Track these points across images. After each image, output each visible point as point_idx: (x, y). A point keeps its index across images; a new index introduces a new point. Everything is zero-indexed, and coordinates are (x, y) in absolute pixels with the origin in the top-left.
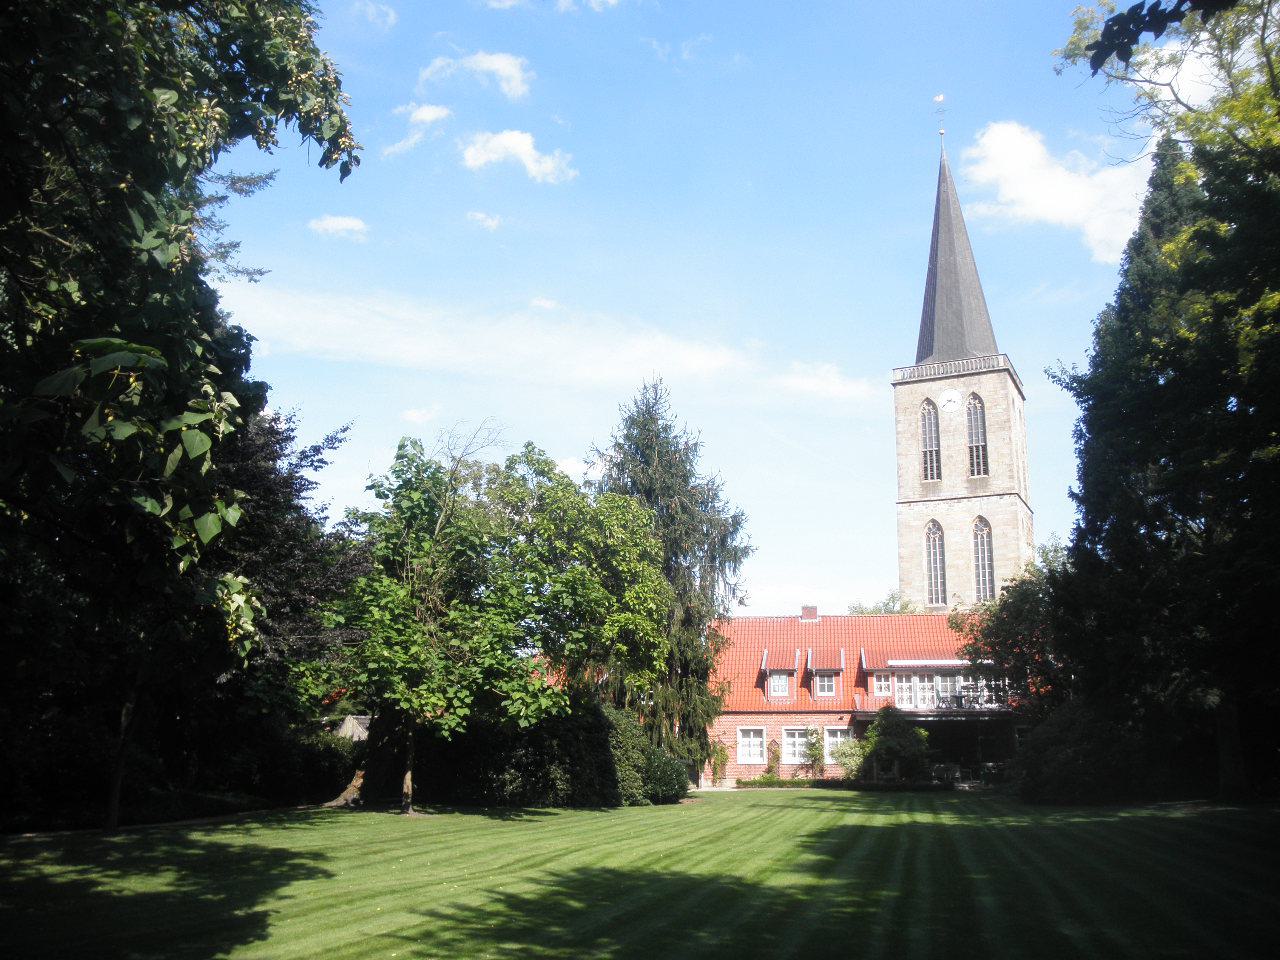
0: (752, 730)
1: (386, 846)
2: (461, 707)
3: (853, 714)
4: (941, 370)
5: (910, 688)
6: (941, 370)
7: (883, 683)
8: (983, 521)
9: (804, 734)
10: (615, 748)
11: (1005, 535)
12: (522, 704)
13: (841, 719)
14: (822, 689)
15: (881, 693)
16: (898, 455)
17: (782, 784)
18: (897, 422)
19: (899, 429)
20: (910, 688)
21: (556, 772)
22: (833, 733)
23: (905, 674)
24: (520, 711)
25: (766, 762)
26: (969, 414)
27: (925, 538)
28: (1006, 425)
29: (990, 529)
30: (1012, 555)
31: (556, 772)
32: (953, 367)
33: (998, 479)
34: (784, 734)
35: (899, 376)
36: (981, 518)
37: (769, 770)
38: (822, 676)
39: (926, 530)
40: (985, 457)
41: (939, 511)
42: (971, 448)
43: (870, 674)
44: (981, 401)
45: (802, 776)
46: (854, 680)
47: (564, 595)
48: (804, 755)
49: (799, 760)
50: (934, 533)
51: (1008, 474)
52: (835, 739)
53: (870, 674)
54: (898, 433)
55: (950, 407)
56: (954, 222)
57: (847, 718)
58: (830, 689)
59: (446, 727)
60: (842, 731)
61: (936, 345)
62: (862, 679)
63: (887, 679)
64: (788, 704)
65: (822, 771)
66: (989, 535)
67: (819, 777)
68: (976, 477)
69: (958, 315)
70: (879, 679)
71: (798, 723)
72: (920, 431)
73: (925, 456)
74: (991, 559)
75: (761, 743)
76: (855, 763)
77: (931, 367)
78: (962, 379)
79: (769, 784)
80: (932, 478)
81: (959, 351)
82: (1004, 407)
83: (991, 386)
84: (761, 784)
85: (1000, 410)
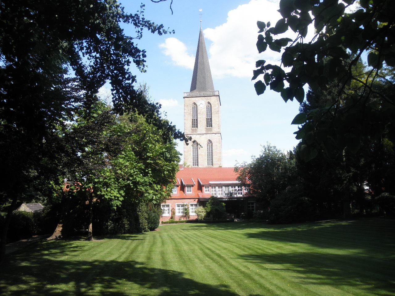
1: (215, 257)
2: (120, 197)
3: (199, 199)
4: (199, 94)
5: (222, 190)
6: (199, 94)
7: (207, 189)
9: (183, 206)
10: (139, 212)
12: (153, 194)
13: (195, 201)
14: (188, 191)
15: (207, 193)
16: (185, 120)
17: (176, 222)
18: (185, 109)
19: (185, 112)
20: (215, 190)
21: (125, 221)
22: (192, 205)
23: (214, 186)
24: (153, 197)
25: (170, 215)
26: (207, 108)
28: (218, 112)
29: (212, 144)
30: (219, 152)
31: (125, 221)
32: (202, 93)
33: (215, 128)
34: (176, 206)
35: (186, 95)
36: (209, 140)
37: (172, 218)
38: (187, 187)
40: (197, 122)
42: (207, 119)
43: (203, 186)
44: (211, 105)
45: (182, 219)
46: (197, 188)
47: (166, 153)
48: (183, 212)
49: (181, 214)
52: (192, 207)
53: (203, 186)
54: (185, 113)
55: (201, 106)
56: (204, 49)
57: (197, 200)
58: (190, 191)
59: (115, 205)
60: (195, 205)
61: (198, 86)
62: (200, 187)
63: (215, 188)
64: (177, 197)
65: (189, 217)
66: (212, 145)
67: (188, 219)
68: (208, 128)
69: (204, 78)
70: (206, 187)
71: (181, 202)
72: (192, 113)
73: (193, 120)
74: (212, 153)
75: (169, 210)
76: (203, 214)
77: (195, 93)
78: (205, 97)
79: (173, 222)
80: (209, 127)
81: (204, 89)
84: (170, 223)
85: (216, 107)
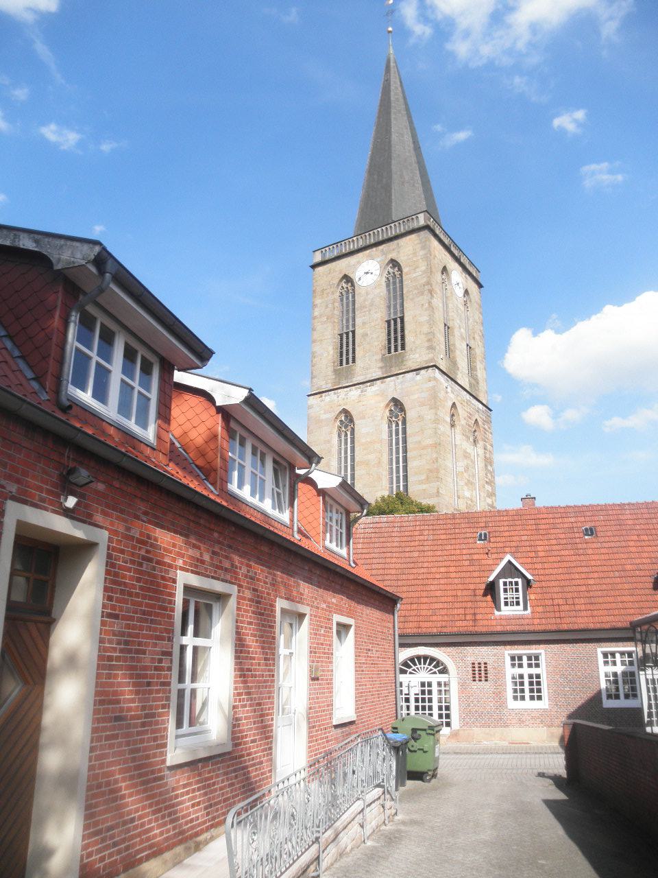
0: (525, 654)
8: (396, 403)
11: (420, 417)
27: (385, 421)
33: (416, 354)
39: (387, 413)
41: (349, 398)
50: (397, 417)
51: (427, 344)
73: (389, 326)
82: (424, 268)
83: (411, 248)
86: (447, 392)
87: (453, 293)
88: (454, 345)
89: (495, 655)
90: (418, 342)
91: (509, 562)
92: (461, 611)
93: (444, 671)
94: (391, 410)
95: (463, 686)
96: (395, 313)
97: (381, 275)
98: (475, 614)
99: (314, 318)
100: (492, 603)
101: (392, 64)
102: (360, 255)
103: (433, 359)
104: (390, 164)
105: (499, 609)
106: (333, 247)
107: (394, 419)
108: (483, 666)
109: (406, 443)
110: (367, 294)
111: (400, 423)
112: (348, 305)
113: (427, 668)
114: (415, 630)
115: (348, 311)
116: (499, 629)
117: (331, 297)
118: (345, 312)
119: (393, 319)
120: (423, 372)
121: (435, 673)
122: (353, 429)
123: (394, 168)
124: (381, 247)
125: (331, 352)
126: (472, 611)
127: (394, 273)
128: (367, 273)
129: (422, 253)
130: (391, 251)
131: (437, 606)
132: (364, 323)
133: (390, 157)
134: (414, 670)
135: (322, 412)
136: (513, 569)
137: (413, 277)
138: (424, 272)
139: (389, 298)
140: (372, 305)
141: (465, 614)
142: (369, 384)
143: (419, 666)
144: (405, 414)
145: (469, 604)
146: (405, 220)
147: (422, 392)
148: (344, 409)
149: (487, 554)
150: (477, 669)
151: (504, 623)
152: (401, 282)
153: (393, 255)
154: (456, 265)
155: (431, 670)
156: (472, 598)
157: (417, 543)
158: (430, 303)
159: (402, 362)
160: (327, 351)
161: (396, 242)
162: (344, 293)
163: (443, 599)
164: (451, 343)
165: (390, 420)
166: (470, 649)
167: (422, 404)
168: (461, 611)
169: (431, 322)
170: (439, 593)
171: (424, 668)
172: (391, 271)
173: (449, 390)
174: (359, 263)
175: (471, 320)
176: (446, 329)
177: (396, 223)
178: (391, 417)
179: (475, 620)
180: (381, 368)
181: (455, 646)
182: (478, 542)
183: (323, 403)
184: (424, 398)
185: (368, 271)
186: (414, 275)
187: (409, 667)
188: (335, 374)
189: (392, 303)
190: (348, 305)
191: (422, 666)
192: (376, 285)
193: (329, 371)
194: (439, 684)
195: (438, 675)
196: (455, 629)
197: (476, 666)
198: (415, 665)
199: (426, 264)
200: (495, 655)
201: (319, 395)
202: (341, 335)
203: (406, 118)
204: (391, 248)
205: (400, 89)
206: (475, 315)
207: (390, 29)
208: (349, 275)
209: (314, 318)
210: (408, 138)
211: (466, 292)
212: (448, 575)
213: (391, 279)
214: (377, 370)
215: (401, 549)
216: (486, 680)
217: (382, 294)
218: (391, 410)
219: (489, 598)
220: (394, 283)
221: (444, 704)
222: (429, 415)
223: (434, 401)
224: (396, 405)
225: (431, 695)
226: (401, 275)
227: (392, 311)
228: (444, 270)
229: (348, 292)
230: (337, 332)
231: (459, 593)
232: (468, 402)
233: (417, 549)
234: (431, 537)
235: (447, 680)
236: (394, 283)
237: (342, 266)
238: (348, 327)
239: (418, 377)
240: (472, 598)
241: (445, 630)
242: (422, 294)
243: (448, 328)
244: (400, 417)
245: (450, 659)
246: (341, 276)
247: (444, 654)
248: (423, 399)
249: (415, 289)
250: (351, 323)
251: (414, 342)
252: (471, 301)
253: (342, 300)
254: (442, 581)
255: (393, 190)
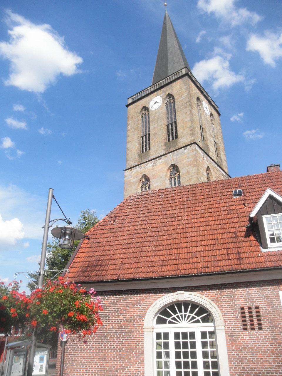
11: (189, 173)
27: (168, 178)
33: (184, 138)
39: (169, 174)
41: (148, 168)
51: (190, 132)
82: (186, 94)
83: (179, 86)
86: (203, 159)
87: (204, 111)
88: (206, 137)
89: (267, 297)
90: (185, 132)
91: (271, 197)
92: (224, 252)
93: (208, 318)
94: (171, 172)
95: (231, 336)
96: (172, 120)
97: (163, 102)
98: (239, 253)
99: (128, 130)
100: (256, 242)
101: (167, 17)
102: (152, 95)
103: (194, 140)
104: (167, 55)
105: (266, 247)
106: (138, 95)
107: (173, 176)
108: (254, 310)
109: (180, 178)
110: (156, 113)
111: (176, 178)
112: (146, 122)
113: (189, 316)
114: (173, 273)
115: (146, 124)
116: (269, 264)
117: (137, 119)
118: (144, 125)
119: (170, 124)
120: (188, 147)
121: (198, 321)
122: (149, 185)
123: (169, 56)
124: (162, 90)
125: (137, 146)
126: (235, 251)
127: (170, 101)
128: (156, 103)
129: (185, 87)
130: (168, 90)
131: (196, 249)
132: (154, 128)
133: (167, 52)
134: (174, 319)
135: (132, 178)
136: (275, 204)
137: (179, 101)
138: (187, 96)
139: (168, 114)
140: (158, 118)
141: (228, 254)
142: (158, 159)
143: (179, 314)
144: (179, 173)
145: (231, 245)
146: (175, 74)
147: (189, 158)
148: (144, 175)
149: (244, 204)
150: (247, 315)
151: (273, 258)
152: (174, 104)
153: (169, 92)
154: (205, 99)
155: (193, 318)
156: (234, 240)
157: (177, 204)
158: (190, 111)
159: (176, 144)
160: (134, 145)
161: (170, 85)
162: (144, 116)
163: (203, 243)
164: (205, 136)
165: (171, 177)
166: (236, 292)
167: (189, 165)
168: (224, 252)
169: (192, 121)
170: (199, 238)
171: (185, 315)
172: (168, 100)
173: (205, 158)
174: (151, 99)
175: (215, 129)
176: (201, 129)
177: (170, 76)
178: (171, 176)
179: (240, 258)
180: (164, 149)
181: (219, 289)
182: (234, 197)
183: (132, 173)
184: (190, 161)
185: (156, 103)
186: (181, 99)
187: (169, 315)
188: (139, 157)
189: (170, 115)
190: (146, 122)
191: (183, 314)
192: (160, 108)
193: (136, 156)
194: (204, 335)
195: (202, 324)
196: (218, 269)
197: (246, 311)
198: (175, 313)
199: (187, 92)
200: (267, 297)
201: (131, 169)
202: (142, 137)
203: (174, 37)
204: (168, 88)
205: (171, 26)
206: (217, 128)
207: (166, 4)
208: (146, 106)
209: (128, 130)
210: (176, 45)
211: (211, 115)
212: (207, 223)
213: (169, 104)
214: (162, 151)
215: (163, 209)
216: (260, 329)
217: (164, 112)
218: (171, 172)
219: (252, 238)
220: (171, 106)
221: (210, 360)
222: (193, 170)
223: (196, 163)
224: (174, 168)
225: (203, 352)
226: (174, 101)
227: (170, 119)
228: (198, 99)
229: (145, 115)
230: (140, 135)
231: (220, 236)
232: (216, 169)
233: (177, 207)
234: (191, 199)
235: (212, 329)
236: (171, 106)
237: (142, 103)
238: (146, 132)
239: (186, 151)
240: (234, 240)
241: (207, 270)
242: (186, 107)
243: (203, 129)
244: (177, 175)
245: (214, 304)
246: (142, 107)
247: (206, 298)
248: (190, 162)
249: (182, 106)
250: (147, 130)
251: (182, 133)
252: (214, 120)
253: (143, 120)
254: (201, 229)
255: (169, 66)
